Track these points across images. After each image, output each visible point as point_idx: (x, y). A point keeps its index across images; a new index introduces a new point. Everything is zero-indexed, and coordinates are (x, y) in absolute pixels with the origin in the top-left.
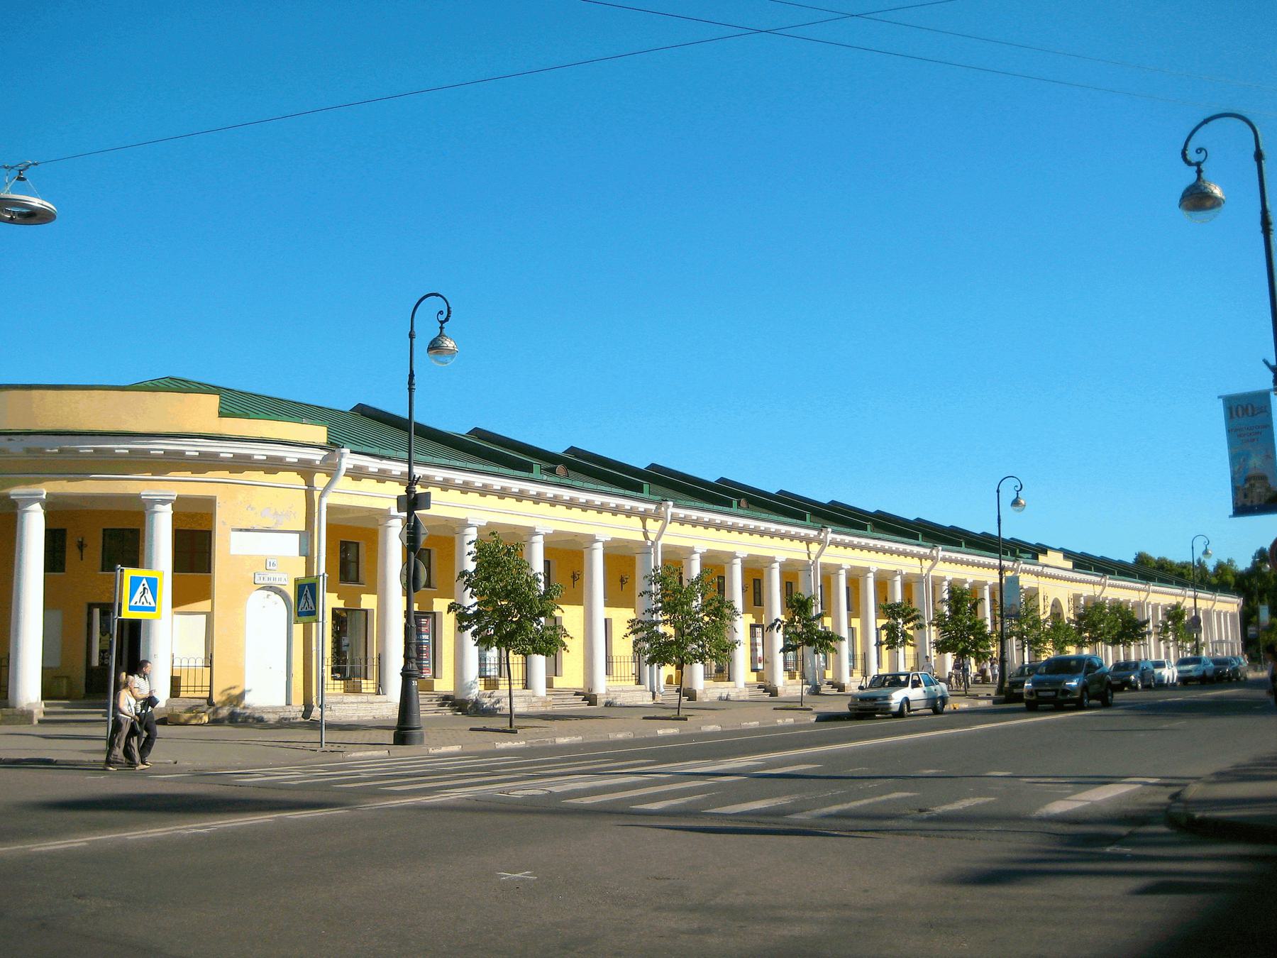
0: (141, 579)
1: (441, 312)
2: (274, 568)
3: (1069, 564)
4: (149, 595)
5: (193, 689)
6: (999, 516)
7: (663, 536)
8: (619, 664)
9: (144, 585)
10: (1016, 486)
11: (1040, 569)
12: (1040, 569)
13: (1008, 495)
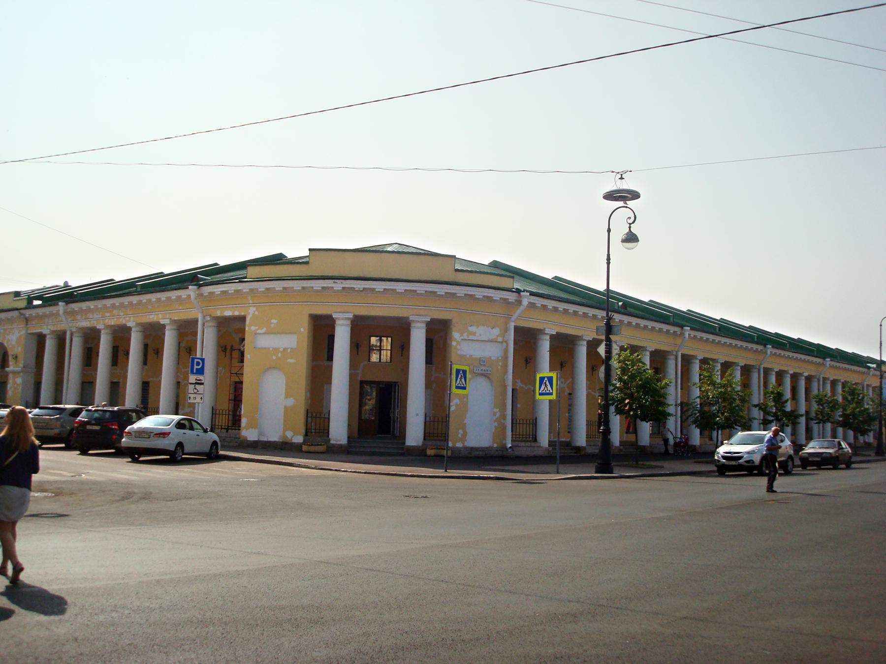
2: (485, 364)
4: (463, 380)
5: (436, 435)
6: (609, 255)
8: (521, 425)
10: (629, 218)
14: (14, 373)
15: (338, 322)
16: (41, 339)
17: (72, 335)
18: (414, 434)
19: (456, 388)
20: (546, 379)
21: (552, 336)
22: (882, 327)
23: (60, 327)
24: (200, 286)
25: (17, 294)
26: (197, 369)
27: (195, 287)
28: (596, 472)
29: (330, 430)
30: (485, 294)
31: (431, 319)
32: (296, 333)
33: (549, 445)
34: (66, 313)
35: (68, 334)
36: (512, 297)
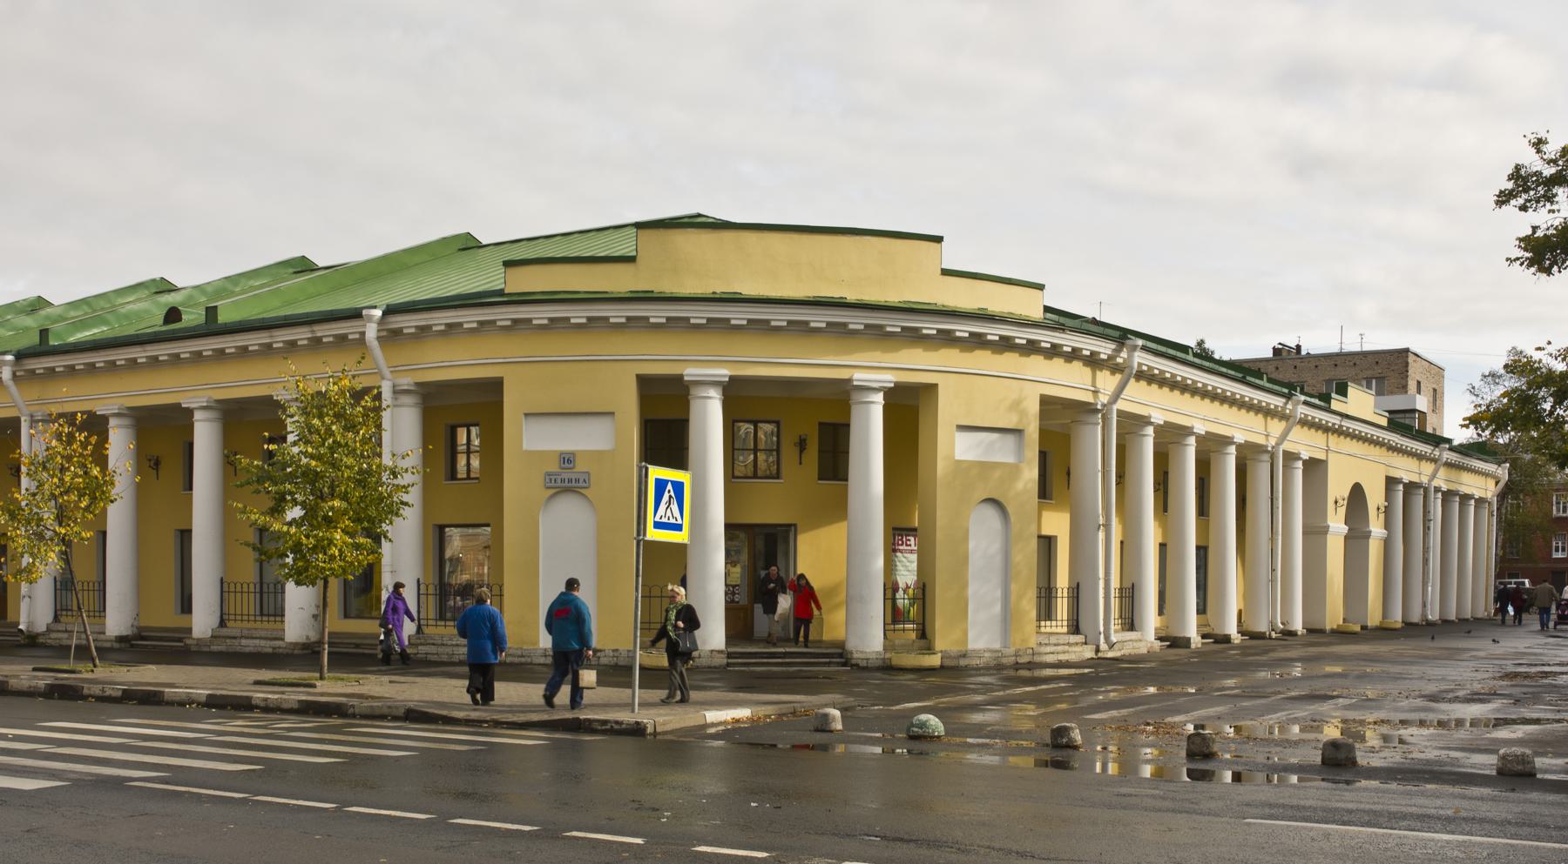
4: (675, 507)
7: (1120, 401)
9: (669, 491)
12: (1335, 420)
19: (655, 527)
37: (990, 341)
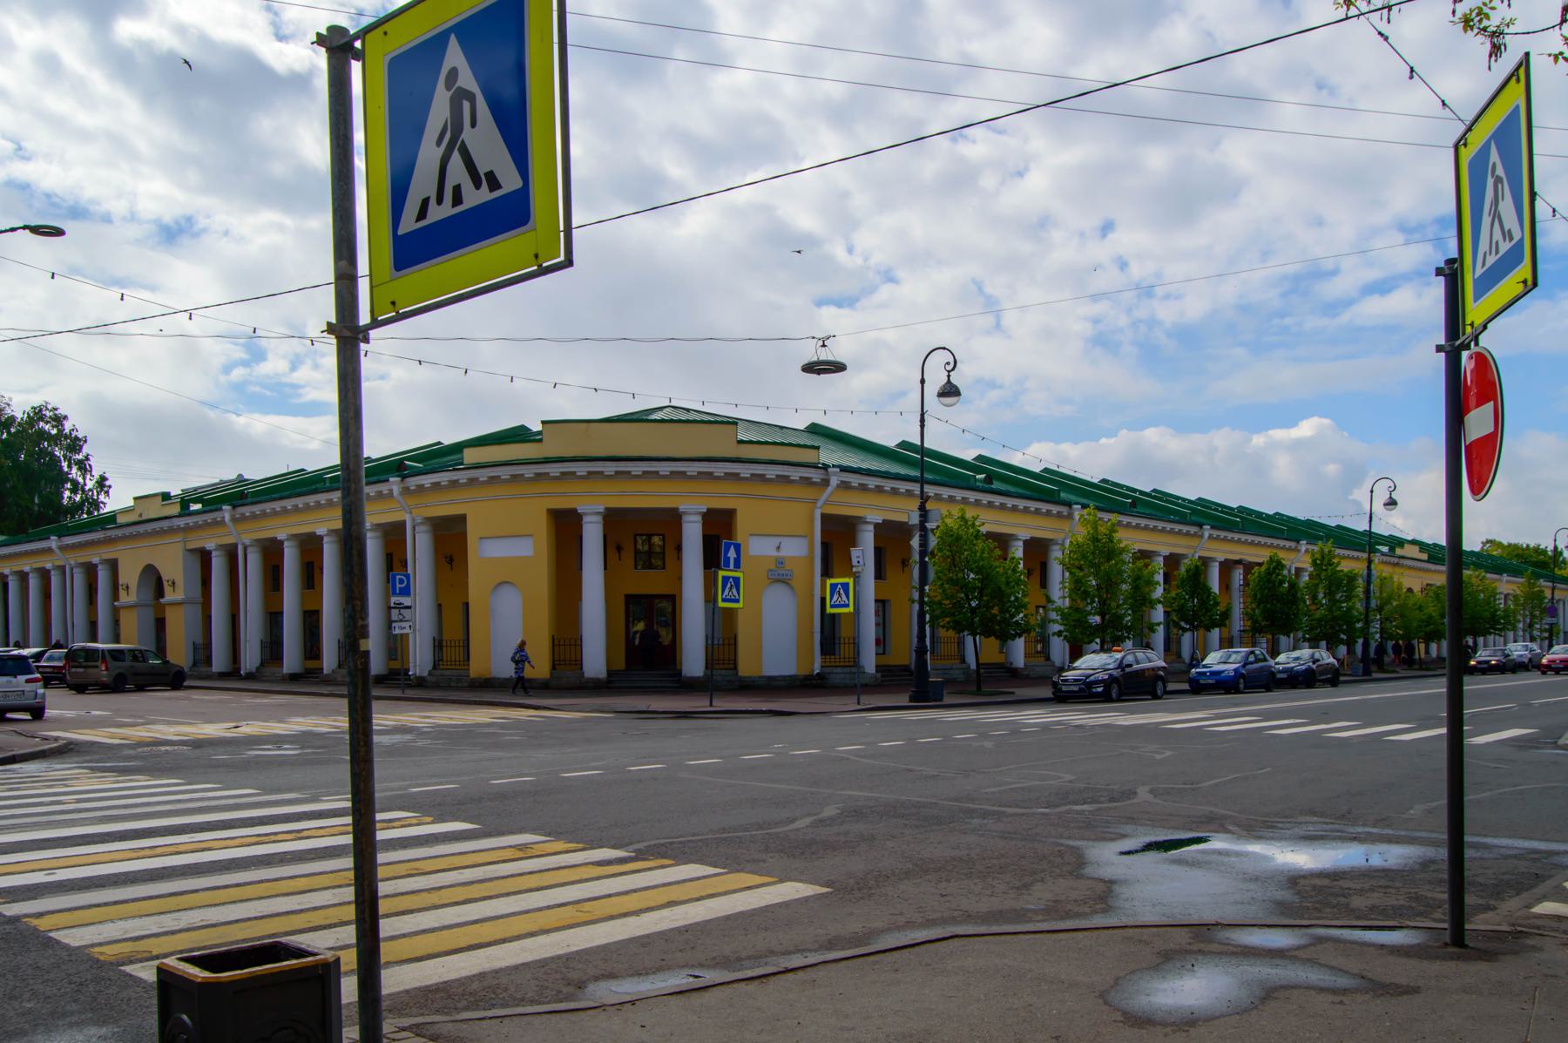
0: (838, 584)
1: (948, 363)
3: (1425, 556)
4: (734, 591)
7: (368, 508)
11: (1396, 560)
12: (1396, 560)
13: (936, 380)
14: (173, 604)
15: (586, 519)
16: (205, 557)
17: (245, 549)
18: (693, 661)
20: (839, 586)
21: (877, 526)
22: (1374, 494)
23: (229, 540)
24: (404, 477)
25: (166, 496)
26: (400, 588)
27: (399, 479)
28: (910, 701)
29: (584, 660)
30: (781, 473)
31: (708, 509)
32: (531, 535)
33: (876, 671)
34: (234, 520)
35: (240, 548)
36: (816, 476)
37: (793, 480)
